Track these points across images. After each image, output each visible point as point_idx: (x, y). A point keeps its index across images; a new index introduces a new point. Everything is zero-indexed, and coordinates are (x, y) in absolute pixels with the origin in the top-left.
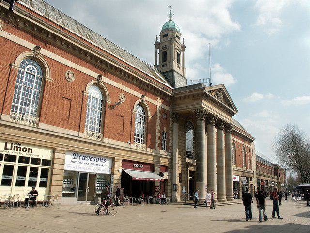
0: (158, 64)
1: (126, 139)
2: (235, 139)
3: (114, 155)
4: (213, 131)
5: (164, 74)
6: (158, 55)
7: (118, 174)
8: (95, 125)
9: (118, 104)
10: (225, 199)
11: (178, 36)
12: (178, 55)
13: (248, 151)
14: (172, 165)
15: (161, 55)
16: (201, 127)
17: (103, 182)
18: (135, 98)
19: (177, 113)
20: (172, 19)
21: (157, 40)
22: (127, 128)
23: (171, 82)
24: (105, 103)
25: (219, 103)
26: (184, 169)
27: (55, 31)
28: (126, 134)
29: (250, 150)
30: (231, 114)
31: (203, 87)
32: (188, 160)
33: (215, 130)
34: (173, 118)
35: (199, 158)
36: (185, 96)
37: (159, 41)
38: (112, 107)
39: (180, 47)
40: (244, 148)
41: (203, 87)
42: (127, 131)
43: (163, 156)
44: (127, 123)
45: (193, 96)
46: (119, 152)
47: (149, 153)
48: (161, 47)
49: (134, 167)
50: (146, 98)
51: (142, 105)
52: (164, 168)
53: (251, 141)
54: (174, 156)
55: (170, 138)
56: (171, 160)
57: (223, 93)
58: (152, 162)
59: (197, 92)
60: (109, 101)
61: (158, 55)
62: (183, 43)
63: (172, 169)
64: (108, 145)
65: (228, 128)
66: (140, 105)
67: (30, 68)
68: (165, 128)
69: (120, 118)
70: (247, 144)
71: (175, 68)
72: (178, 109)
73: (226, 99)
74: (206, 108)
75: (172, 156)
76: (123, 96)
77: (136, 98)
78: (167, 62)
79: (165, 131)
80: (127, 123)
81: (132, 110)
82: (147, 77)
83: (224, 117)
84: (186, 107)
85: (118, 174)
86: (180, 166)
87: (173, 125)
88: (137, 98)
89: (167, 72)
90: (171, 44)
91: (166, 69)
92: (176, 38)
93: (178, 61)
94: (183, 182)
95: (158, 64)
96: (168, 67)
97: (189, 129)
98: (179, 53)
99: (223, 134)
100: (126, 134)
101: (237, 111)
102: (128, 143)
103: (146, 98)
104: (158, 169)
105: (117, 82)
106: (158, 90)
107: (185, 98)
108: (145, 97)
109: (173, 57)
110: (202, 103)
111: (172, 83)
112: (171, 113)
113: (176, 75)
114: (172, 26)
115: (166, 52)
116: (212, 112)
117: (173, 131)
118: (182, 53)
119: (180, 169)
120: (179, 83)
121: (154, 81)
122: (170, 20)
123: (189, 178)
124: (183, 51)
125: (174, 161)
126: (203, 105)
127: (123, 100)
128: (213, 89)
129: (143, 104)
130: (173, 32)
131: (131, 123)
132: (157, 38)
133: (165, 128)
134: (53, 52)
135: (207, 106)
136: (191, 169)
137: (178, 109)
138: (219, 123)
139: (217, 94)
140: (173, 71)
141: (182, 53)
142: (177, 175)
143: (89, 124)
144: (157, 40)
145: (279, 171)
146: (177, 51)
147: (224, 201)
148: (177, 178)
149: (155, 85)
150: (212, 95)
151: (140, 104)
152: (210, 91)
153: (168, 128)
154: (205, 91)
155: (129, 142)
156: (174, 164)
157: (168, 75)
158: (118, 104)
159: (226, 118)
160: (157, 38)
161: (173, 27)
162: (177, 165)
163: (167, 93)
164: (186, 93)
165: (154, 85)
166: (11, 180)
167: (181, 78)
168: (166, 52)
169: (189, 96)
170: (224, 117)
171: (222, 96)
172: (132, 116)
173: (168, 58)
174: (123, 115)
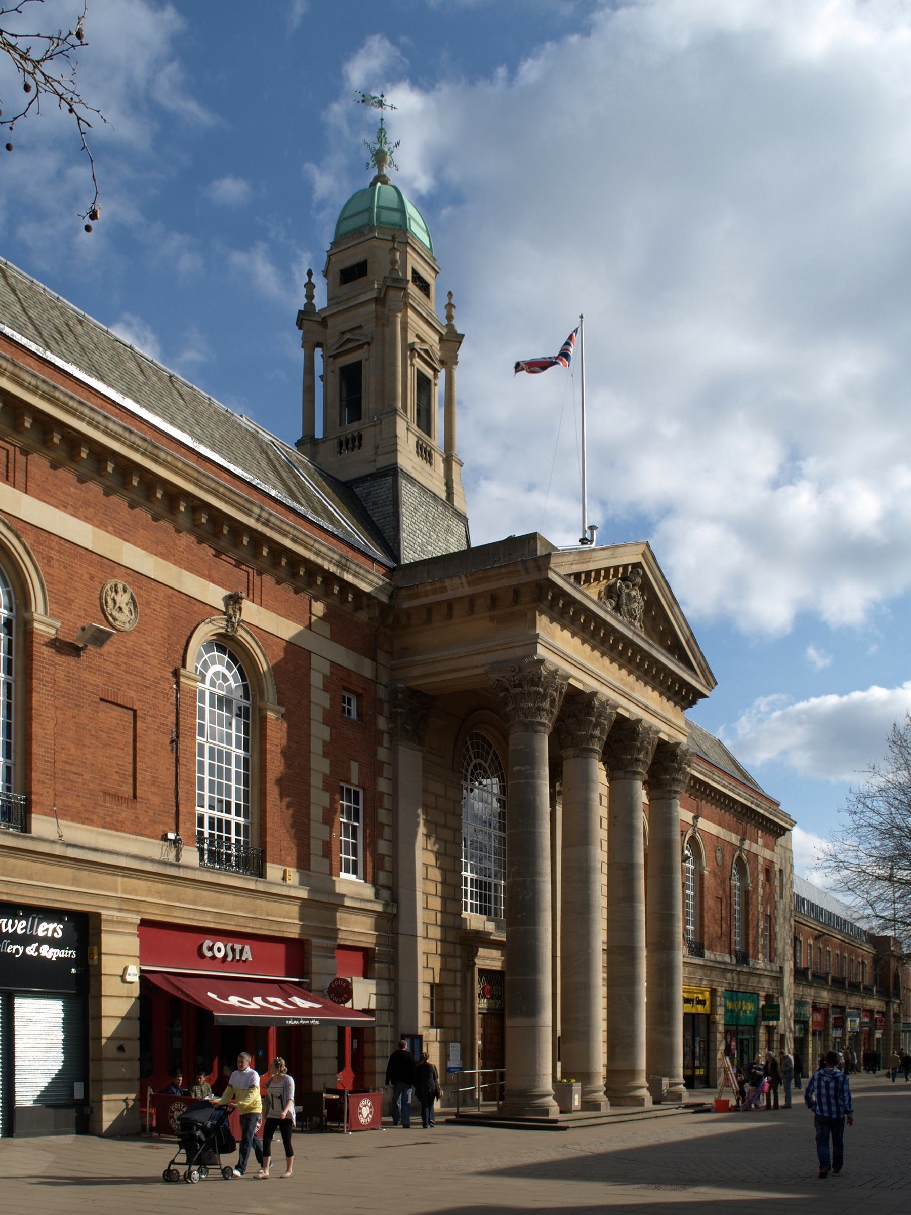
0: (319, 434)
1: (153, 822)
2: (703, 824)
3: (94, 902)
4: (586, 781)
5: (348, 492)
6: (319, 385)
7: (123, 989)
8: (228, 811)
9: (100, 638)
10: (644, 1093)
11: (427, 274)
12: (424, 385)
13: (761, 877)
14: (395, 946)
15: (335, 379)
16: (530, 760)
17: (827, 1088)
18: (192, 611)
19: (414, 693)
20: (386, 170)
21: (310, 297)
22: (156, 764)
23: (388, 534)
24: (28, 633)
25: (621, 637)
26: (457, 963)
27: (132, 447)
28: (154, 797)
29: (768, 872)
30: (685, 696)
31: (541, 551)
32: (475, 921)
33: (600, 773)
34: (392, 718)
35: (520, 913)
36: (450, 604)
37: (321, 301)
38: (66, 648)
39: (433, 339)
40: (741, 864)
41: (541, 551)
42: (154, 782)
43: (348, 902)
44: (154, 738)
45: (494, 599)
46: (121, 886)
47: (190, 874)
48: (332, 339)
49: (203, 956)
50: (250, 612)
51: (230, 646)
52: (358, 958)
53: (776, 830)
54: (403, 902)
55: (383, 816)
56: (393, 921)
57: (646, 587)
58: (293, 932)
59: (516, 574)
60: (45, 625)
61: (319, 385)
62: (450, 317)
63: (393, 961)
64: (58, 850)
65: (665, 764)
66: (222, 649)
67: (216, 674)
68: (354, 766)
69: (117, 712)
70: (757, 847)
71: (407, 458)
72: (417, 671)
73: (659, 616)
74: (553, 660)
75: (394, 899)
76: (123, 599)
77: (198, 610)
78: (365, 420)
79: (355, 779)
80: (154, 738)
81: (176, 674)
82: (255, 498)
83: (646, 709)
84: (455, 655)
85: (123, 989)
86: (432, 947)
87: (393, 749)
88: (205, 610)
89: (362, 479)
90: (384, 322)
91: (355, 465)
92: (412, 289)
93: (424, 421)
94: (448, 1020)
95: (319, 434)
96: (366, 451)
97: (480, 772)
98: (429, 373)
99: (642, 796)
100: (154, 797)
101: (711, 682)
102: (165, 838)
103: (250, 612)
104: (323, 969)
105: (86, 519)
106: (314, 569)
107: (450, 616)
108: (246, 604)
109: (394, 398)
110: (534, 641)
111: (384, 530)
112: (382, 693)
113: (408, 494)
114: (387, 217)
115: (358, 365)
116: (584, 682)
117: (394, 781)
118: (442, 374)
119: (436, 963)
120: (423, 538)
121: (291, 519)
122: (381, 178)
123: (482, 1004)
124: (449, 362)
125: (403, 927)
126: (542, 652)
127: (125, 619)
128: (592, 566)
129: (234, 639)
130: (394, 249)
131: (175, 742)
132: (310, 286)
133: (354, 766)
134: (44, 495)
135: (560, 650)
136: (489, 959)
137: (417, 671)
138: (624, 736)
139: (611, 592)
140: (393, 472)
141: (442, 374)
142: (423, 991)
143: (206, 809)
144: (310, 297)
145: (893, 964)
146: (418, 362)
147: (640, 1101)
148: (423, 1006)
149: (295, 540)
150: (590, 596)
151: (225, 643)
152: (577, 576)
153: (373, 769)
154: (552, 576)
155: (171, 836)
156: (402, 940)
157: (371, 497)
158: (100, 638)
159: (655, 714)
160: (310, 286)
161: (396, 217)
162: (422, 946)
163: (313, 557)
164: (458, 587)
165: (288, 543)
166: (694, 1088)
167: (436, 511)
168: (358, 365)
169: (471, 601)
170: (646, 709)
171: (638, 606)
172: (181, 707)
173: (369, 403)
174: (130, 695)
